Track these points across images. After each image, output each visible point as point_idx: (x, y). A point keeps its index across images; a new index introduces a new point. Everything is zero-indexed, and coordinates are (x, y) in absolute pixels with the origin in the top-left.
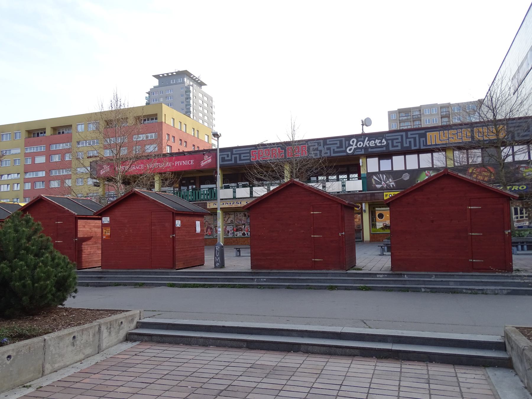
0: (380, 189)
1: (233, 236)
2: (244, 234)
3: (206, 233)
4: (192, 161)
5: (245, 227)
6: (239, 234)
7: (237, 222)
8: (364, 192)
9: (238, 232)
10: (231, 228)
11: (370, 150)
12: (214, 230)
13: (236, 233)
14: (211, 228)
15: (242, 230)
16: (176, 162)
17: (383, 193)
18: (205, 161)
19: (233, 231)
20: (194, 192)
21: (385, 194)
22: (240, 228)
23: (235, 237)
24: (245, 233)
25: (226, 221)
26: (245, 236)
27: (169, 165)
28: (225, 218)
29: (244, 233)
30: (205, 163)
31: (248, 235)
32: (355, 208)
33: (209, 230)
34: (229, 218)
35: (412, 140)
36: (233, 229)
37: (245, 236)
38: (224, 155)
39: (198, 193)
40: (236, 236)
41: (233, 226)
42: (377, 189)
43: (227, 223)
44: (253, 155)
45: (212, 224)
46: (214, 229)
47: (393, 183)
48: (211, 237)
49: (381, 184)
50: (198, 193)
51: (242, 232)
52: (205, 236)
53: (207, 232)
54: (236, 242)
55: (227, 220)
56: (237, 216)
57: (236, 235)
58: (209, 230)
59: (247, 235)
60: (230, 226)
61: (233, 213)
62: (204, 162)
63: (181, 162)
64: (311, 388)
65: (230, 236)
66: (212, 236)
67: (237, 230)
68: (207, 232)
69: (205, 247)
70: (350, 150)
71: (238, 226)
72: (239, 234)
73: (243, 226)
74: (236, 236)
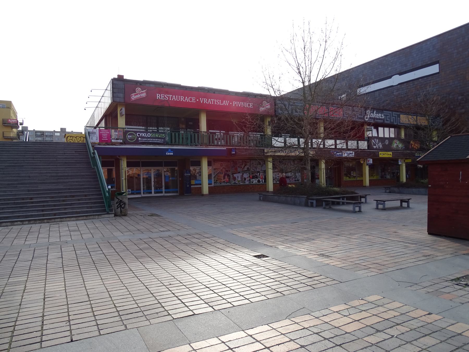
0: (376, 149)
1: (250, 183)
2: (259, 181)
3: (223, 180)
4: (194, 99)
5: (259, 174)
6: (255, 181)
7: (253, 170)
8: (368, 151)
9: (254, 179)
10: (247, 175)
11: (376, 120)
12: (232, 177)
13: (252, 180)
14: (228, 175)
15: (257, 178)
16: (235, 103)
17: (379, 152)
18: (137, 94)
19: (249, 178)
20: (173, 134)
21: (380, 153)
22: (256, 175)
23: (251, 184)
24: (260, 180)
25: (243, 168)
26: (260, 183)
27: (226, 104)
28: (241, 165)
29: (259, 180)
30: (137, 96)
31: (262, 182)
32: (418, 165)
33: (226, 177)
34: (245, 165)
35: (394, 118)
36: (249, 176)
37: (260, 183)
38: (388, 113)
39: (198, 135)
40: (252, 183)
41: (249, 173)
42: (374, 149)
43: (244, 170)
44: (392, 116)
45: (229, 171)
46: (232, 176)
47: (381, 146)
48: (228, 184)
49: (375, 145)
50: (198, 135)
51: (257, 179)
52: (222, 184)
53: (224, 179)
54: (253, 188)
55: (244, 167)
56: (253, 163)
57: (253, 183)
58: (226, 177)
59: (261, 182)
60: (247, 173)
61: (249, 161)
62: (135, 95)
63: (240, 103)
64: (19, 313)
65: (247, 183)
66: (229, 183)
67: (253, 178)
68: (224, 179)
69: (202, 193)
70: (367, 118)
71: (254, 173)
72: (255, 181)
73: (258, 174)
74: (252, 183)
